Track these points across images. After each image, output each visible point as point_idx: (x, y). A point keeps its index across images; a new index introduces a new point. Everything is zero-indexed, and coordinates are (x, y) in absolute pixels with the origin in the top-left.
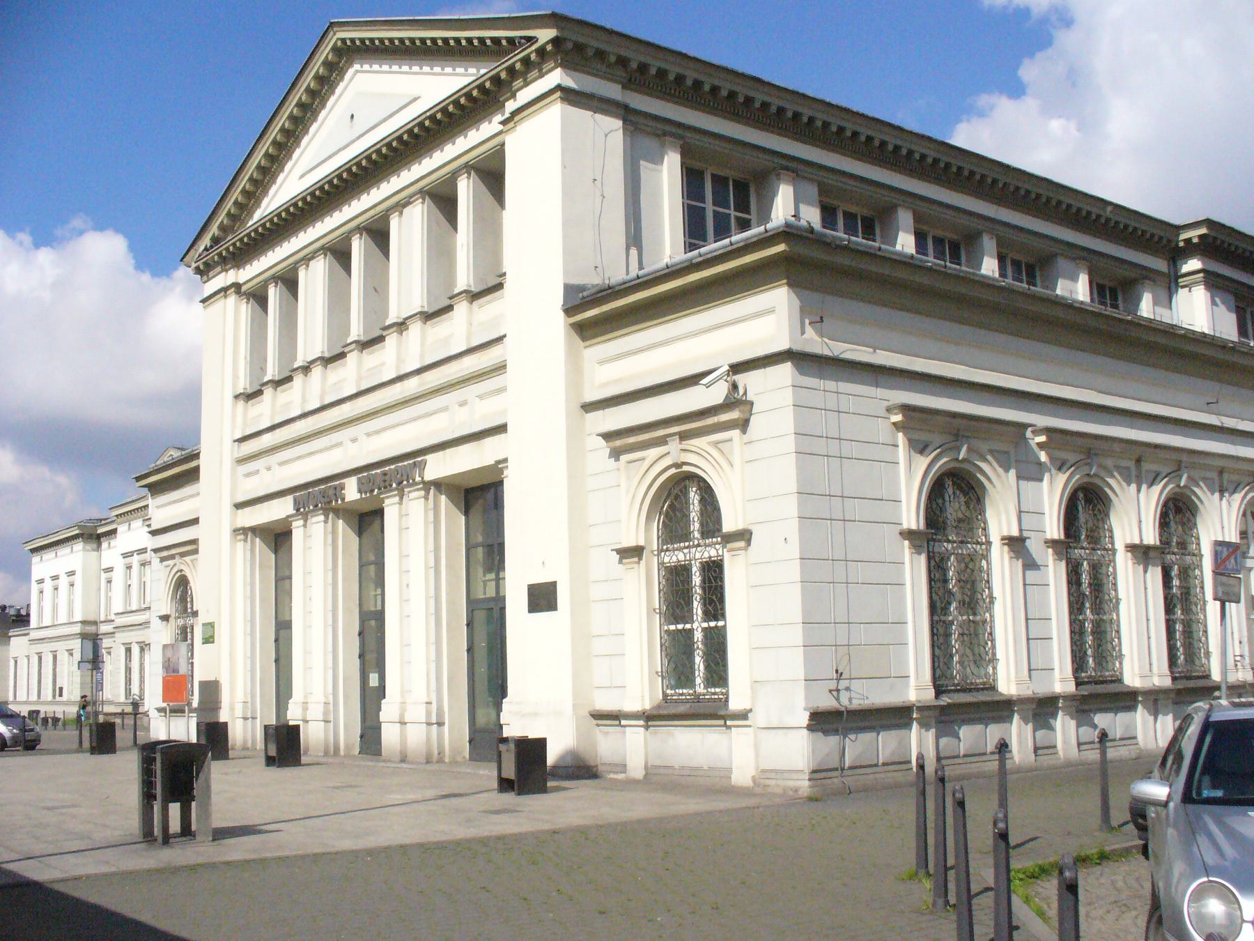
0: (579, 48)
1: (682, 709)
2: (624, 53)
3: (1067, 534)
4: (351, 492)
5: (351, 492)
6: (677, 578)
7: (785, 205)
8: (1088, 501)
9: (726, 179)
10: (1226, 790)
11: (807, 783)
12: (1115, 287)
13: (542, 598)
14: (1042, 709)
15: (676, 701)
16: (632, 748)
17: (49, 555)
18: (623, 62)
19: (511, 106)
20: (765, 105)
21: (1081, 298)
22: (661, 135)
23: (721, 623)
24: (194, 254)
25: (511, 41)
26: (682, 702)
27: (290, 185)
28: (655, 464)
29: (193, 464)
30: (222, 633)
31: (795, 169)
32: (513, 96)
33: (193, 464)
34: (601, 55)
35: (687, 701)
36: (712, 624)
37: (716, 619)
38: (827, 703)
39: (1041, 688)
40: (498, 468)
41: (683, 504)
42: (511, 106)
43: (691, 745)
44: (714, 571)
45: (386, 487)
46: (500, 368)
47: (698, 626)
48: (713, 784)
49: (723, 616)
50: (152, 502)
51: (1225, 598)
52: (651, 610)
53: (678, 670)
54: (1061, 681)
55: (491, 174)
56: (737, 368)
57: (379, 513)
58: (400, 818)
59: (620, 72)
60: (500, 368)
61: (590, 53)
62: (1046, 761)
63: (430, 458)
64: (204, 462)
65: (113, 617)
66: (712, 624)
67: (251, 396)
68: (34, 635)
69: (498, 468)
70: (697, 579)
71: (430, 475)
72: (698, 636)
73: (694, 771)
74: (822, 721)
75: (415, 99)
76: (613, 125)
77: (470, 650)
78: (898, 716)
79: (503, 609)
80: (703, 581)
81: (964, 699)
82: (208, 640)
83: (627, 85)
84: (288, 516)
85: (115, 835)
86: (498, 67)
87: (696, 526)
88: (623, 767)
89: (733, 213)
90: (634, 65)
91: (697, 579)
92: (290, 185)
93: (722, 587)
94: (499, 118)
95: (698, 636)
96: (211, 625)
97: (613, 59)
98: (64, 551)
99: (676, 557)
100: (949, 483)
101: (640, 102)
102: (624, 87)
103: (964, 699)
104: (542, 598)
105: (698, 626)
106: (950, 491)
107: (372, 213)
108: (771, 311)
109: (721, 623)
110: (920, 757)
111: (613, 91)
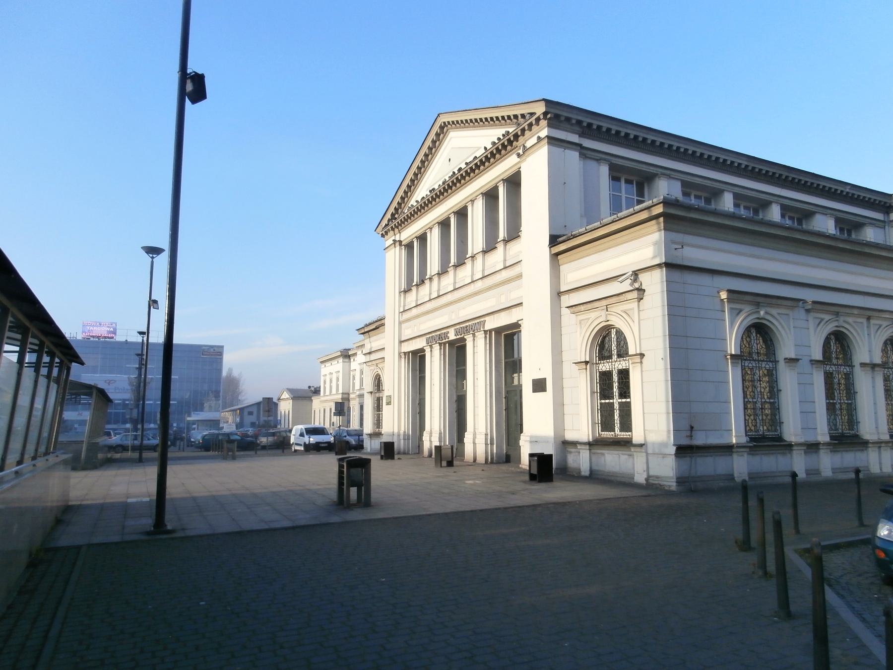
0: (557, 117)
2: (580, 118)
3: (824, 357)
6: (606, 376)
7: (664, 188)
8: (837, 339)
9: (619, 356)
11: (675, 484)
12: (848, 225)
13: (539, 386)
14: (812, 447)
16: (582, 461)
17: (328, 364)
18: (579, 122)
20: (653, 142)
21: (830, 232)
22: (598, 160)
24: (380, 228)
27: (422, 192)
28: (596, 319)
30: (395, 401)
31: (669, 174)
34: (568, 120)
36: (624, 400)
37: (625, 398)
38: (685, 442)
39: (811, 439)
40: (517, 326)
41: (607, 343)
44: (624, 374)
46: (520, 276)
47: (616, 401)
48: (625, 482)
49: (629, 397)
50: (367, 342)
52: (592, 393)
53: (607, 424)
54: (823, 436)
55: (514, 182)
56: (636, 274)
58: (470, 490)
59: (577, 128)
60: (520, 276)
61: (563, 119)
62: (814, 478)
63: (487, 318)
64: (386, 321)
66: (624, 400)
67: (407, 291)
68: (323, 399)
69: (517, 326)
70: (615, 378)
71: (488, 327)
72: (616, 406)
73: (614, 474)
74: (682, 451)
76: (574, 155)
78: (728, 449)
79: (521, 391)
80: (619, 379)
81: (766, 439)
82: (388, 403)
83: (582, 135)
87: (615, 352)
88: (579, 471)
89: (636, 198)
90: (585, 124)
91: (615, 378)
92: (422, 192)
93: (629, 382)
95: (616, 406)
96: (390, 396)
97: (574, 121)
98: (334, 362)
99: (605, 366)
101: (588, 143)
102: (580, 136)
103: (766, 439)
104: (539, 386)
105: (616, 401)
106: (754, 334)
110: (399, 432)
111: (574, 138)
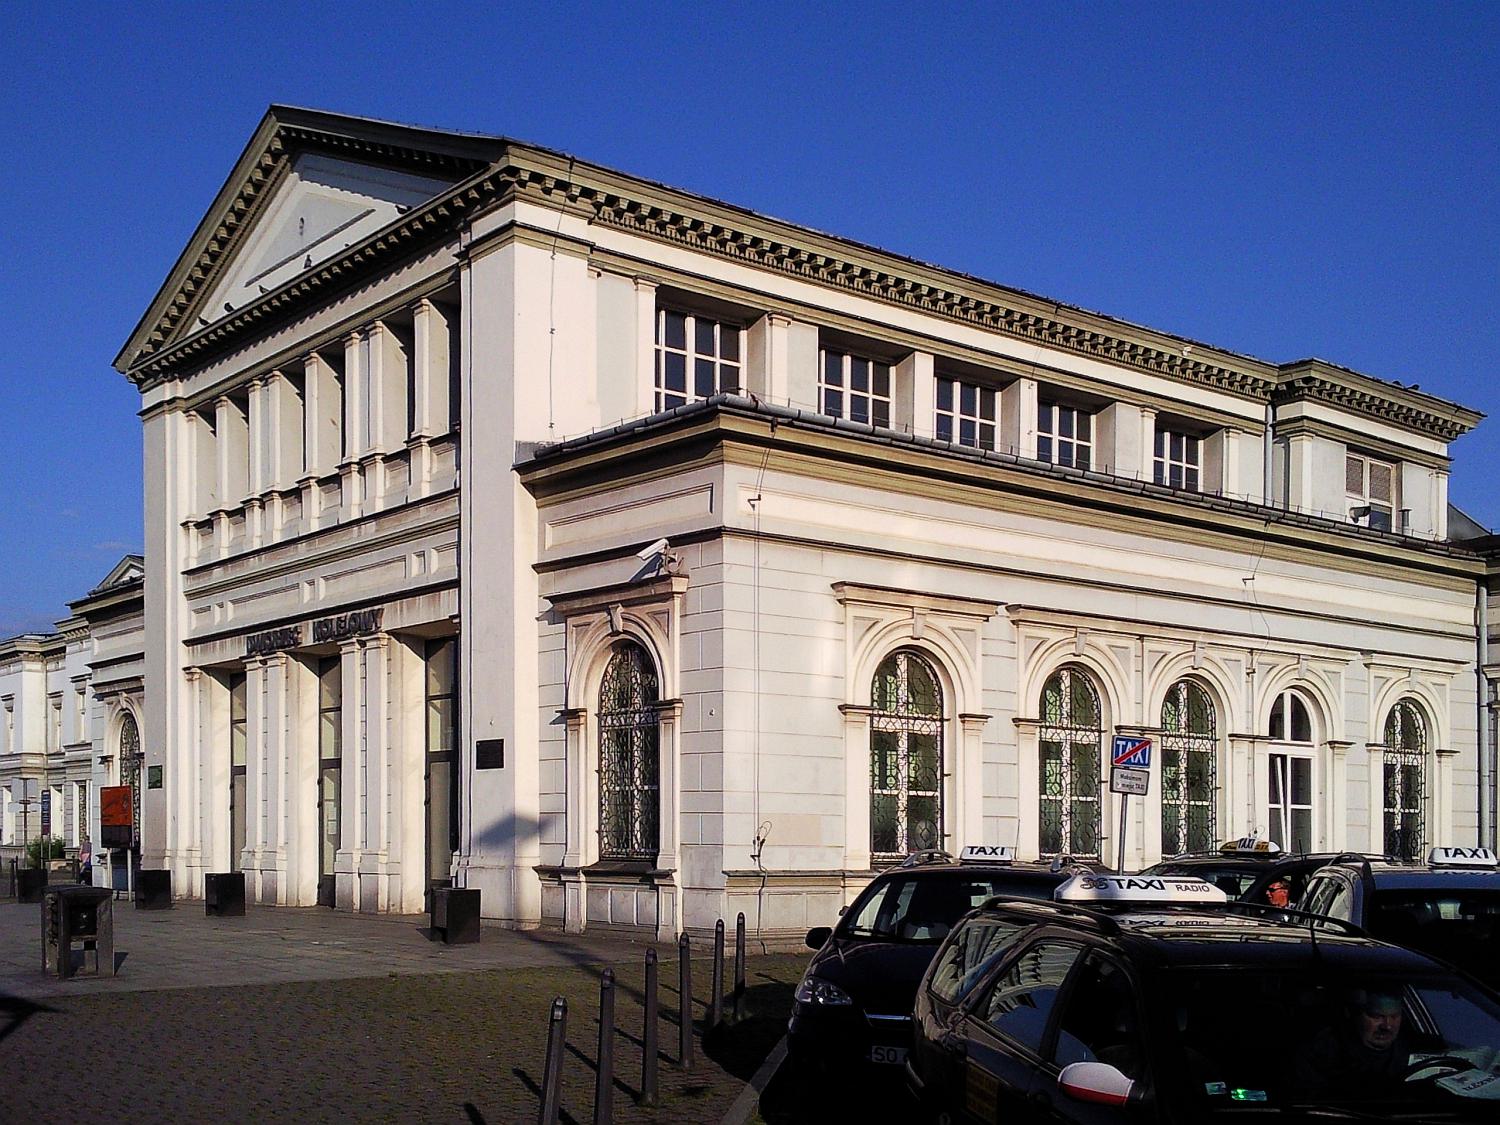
1: (618, 866)
4: (307, 639)
5: (307, 639)
10: (930, 926)
15: (613, 860)
19: (466, 239)
23: (1386, 810)
25: (464, 162)
26: (617, 860)
27: (236, 291)
29: (137, 595)
32: (468, 228)
33: (137, 595)
35: (623, 860)
42: (466, 239)
43: (627, 901)
45: (344, 635)
51: (1127, 790)
57: (336, 659)
65: (63, 750)
75: (369, 212)
77: (427, 802)
84: (242, 658)
85: (731, 466)
86: (451, 191)
94: (456, 248)
100: (903, 665)
107: (326, 337)
108: (819, 412)
109: (1386, 810)
